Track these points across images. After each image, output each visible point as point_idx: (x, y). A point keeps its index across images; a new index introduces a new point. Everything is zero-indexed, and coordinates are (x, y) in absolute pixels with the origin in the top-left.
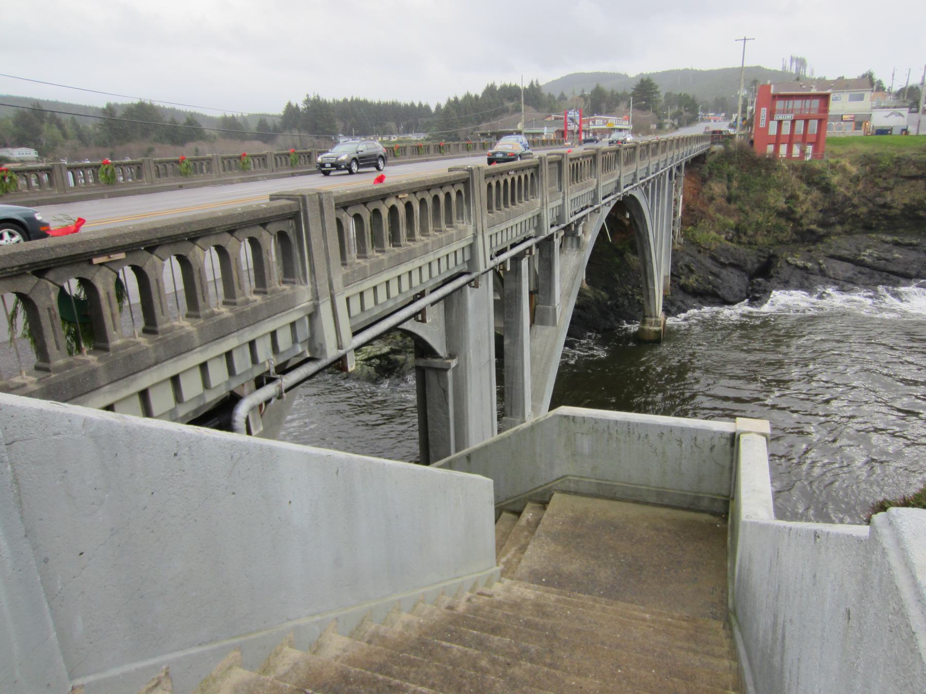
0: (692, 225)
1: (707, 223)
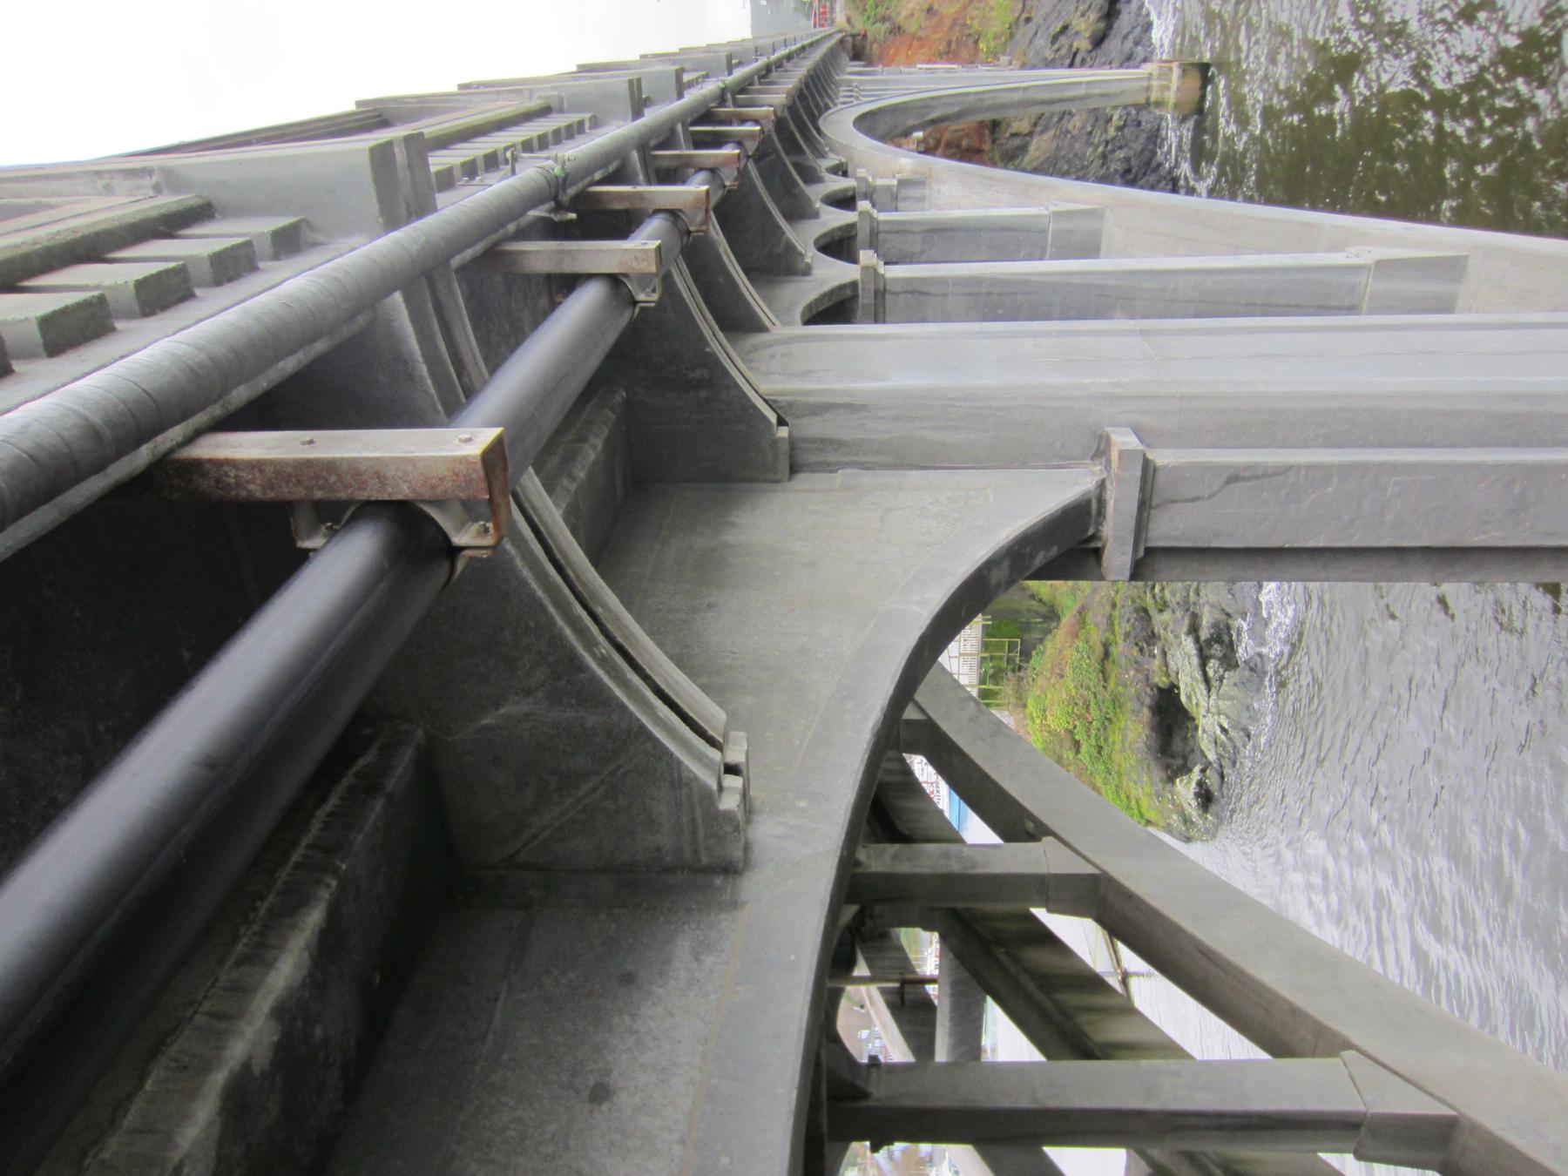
0: (976, 42)
1: (975, 13)
